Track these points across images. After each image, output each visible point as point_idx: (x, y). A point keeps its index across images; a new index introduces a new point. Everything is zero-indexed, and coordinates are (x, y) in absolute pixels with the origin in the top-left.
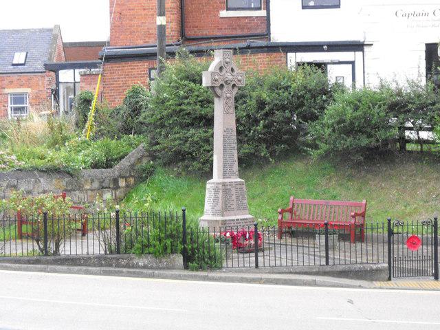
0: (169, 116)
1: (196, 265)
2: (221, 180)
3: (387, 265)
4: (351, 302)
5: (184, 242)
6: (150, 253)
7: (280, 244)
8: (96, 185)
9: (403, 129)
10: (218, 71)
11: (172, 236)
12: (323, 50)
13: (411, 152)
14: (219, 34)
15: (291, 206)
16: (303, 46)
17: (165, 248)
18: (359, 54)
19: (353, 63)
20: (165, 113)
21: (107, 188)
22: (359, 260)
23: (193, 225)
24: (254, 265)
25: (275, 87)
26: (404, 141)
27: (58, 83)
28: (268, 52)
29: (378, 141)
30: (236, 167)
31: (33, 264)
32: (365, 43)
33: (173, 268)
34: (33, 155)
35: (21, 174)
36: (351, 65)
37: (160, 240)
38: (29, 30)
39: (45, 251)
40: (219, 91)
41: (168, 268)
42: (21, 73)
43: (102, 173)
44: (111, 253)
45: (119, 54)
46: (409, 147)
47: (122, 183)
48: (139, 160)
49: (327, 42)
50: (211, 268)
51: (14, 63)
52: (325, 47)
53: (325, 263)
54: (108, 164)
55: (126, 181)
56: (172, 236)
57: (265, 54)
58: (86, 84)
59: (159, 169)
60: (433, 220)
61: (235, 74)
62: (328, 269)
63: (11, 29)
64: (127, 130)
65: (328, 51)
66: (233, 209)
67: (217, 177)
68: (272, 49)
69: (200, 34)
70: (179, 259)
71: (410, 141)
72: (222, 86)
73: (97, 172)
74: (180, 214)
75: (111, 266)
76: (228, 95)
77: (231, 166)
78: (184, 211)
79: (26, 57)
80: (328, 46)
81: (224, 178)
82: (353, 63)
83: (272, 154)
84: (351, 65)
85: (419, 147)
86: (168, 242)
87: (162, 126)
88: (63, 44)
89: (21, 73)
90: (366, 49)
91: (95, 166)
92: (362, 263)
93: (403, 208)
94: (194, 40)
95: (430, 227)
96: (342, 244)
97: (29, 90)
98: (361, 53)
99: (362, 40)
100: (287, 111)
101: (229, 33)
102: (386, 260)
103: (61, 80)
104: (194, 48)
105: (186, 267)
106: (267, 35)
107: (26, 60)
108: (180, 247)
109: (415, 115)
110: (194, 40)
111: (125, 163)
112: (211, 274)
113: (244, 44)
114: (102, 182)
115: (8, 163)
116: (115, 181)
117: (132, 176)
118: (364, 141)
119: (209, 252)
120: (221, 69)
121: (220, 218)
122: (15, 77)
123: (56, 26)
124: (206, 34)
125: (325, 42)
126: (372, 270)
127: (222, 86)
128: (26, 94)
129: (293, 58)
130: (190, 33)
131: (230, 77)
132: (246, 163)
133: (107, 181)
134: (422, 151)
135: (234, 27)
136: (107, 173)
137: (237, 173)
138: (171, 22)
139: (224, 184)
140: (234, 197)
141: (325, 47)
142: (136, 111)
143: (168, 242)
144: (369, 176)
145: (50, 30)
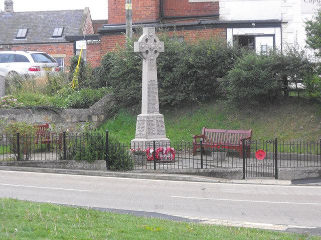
0: (128, 73)
1: (114, 167)
2: (146, 115)
3: (242, 169)
4: (203, 189)
5: (107, 152)
6: (85, 160)
7: (210, 161)
8: (75, 119)
9: (286, 82)
10: (145, 42)
11: (99, 149)
12: (252, 27)
13: (292, 97)
14: (189, 14)
15: (249, 136)
16: (264, 23)
17: (94, 156)
18: (278, 29)
19: (273, 36)
20: (126, 70)
21: (83, 121)
22: (231, 166)
23: (113, 142)
24: (153, 168)
25: (199, 53)
26: (287, 90)
27: (75, 50)
28: (213, 28)
29: (265, 90)
30: (157, 106)
31: (10, 166)
32: (283, 21)
33: (100, 169)
34: (31, 99)
35: (19, 111)
36: (272, 37)
37: (91, 151)
38: (66, 11)
39: (18, 158)
40: (145, 55)
41: (96, 169)
42: (59, 43)
43: (80, 112)
44: (61, 159)
45: (110, 29)
46: (292, 94)
47: (95, 119)
48: (109, 103)
49: (256, 21)
50: (129, 169)
51: (54, 35)
52: (253, 24)
53: (200, 167)
54: (86, 106)
55: (98, 117)
56: (99, 149)
57: (211, 29)
58: (91, 51)
59: (122, 109)
60: (274, 140)
61: (157, 43)
62: (202, 171)
63: (53, 10)
64: (102, 83)
65: (256, 27)
66: (154, 134)
67: (144, 113)
68: (190, 27)
69: (174, 14)
70: (103, 164)
71: (292, 90)
72: (147, 52)
73: (76, 110)
74: (105, 134)
75: (60, 168)
76: (152, 58)
77: (154, 105)
78: (107, 132)
79: (63, 31)
80: (255, 23)
81: (148, 113)
82: (273, 36)
83: (200, 98)
84: (272, 37)
85: (300, 95)
86: (96, 152)
87: (124, 80)
88: (92, 21)
89: (59, 43)
90: (283, 25)
91: (76, 106)
92: (222, 168)
93: (279, 135)
94: (173, 18)
95: (272, 145)
96: (230, 159)
97: (64, 56)
98: (280, 28)
99: (280, 19)
100: (206, 70)
101: (195, 13)
102: (242, 166)
103: (77, 48)
104: (167, 25)
105: (109, 169)
106: (217, 16)
107: (62, 33)
108: (104, 155)
109: (292, 72)
110: (173, 18)
111: (98, 104)
112: (123, 173)
113: (196, 22)
114: (79, 118)
115: (10, 104)
116: (90, 118)
117: (103, 114)
118: (257, 91)
119: (123, 159)
120: (147, 40)
121: (145, 140)
122: (54, 46)
123: (86, 8)
124: (179, 15)
125: (253, 21)
126: (231, 172)
127: (147, 52)
128: (62, 58)
129: (231, 33)
130: (167, 14)
131: (153, 46)
132: (166, 107)
133: (83, 117)
134: (299, 97)
135: (199, 9)
136: (84, 111)
137: (158, 110)
138: (151, 7)
139: (148, 117)
140: (155, 126)
141: (253, 24)
142: (108, 68)
143: (96, 152)
144: (260, 114)
145: (82, 11)
